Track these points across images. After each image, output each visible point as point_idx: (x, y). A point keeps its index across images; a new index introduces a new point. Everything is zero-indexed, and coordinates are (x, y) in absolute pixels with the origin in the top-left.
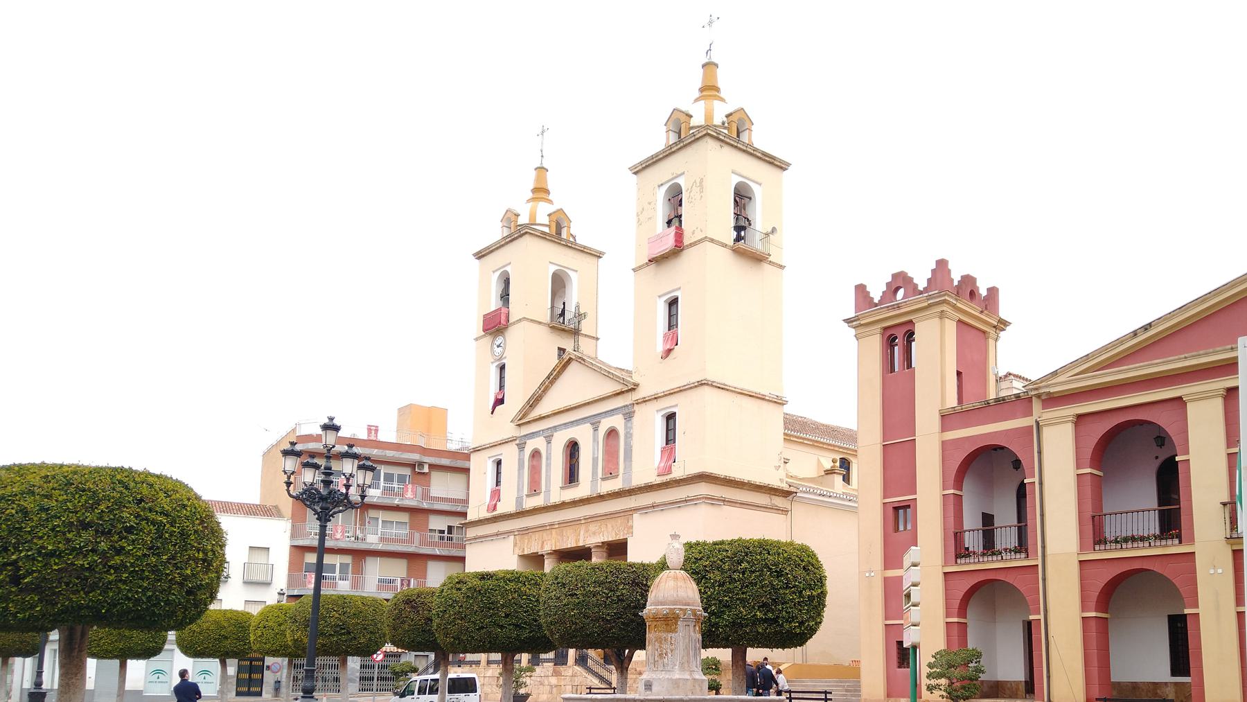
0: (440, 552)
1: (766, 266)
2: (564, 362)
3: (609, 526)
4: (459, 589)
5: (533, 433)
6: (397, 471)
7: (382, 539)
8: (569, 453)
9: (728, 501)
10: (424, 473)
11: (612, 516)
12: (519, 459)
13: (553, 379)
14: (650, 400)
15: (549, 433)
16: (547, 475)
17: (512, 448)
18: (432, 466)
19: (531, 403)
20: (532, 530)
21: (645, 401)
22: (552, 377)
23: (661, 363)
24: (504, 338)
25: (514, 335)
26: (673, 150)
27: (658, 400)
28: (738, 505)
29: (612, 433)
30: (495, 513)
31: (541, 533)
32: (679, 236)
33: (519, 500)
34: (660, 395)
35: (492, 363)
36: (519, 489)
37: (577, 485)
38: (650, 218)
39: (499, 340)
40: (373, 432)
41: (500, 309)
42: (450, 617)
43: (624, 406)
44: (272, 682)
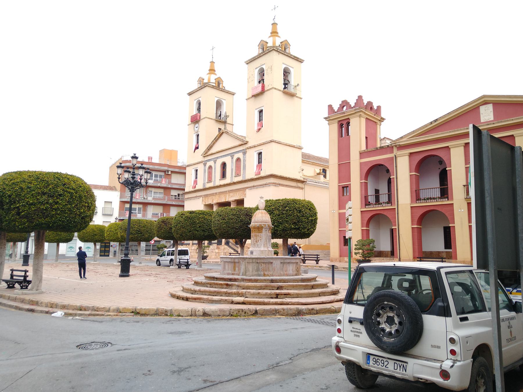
1: (295, 98)
2: (221, 133)
3: (237, 194)
4: (182, 217)
6: (159, 174)
7: (153, 199)
8: (222, 167)
9: (281, 185)
10: (169, 174)
12: (204, 169)
13: (216, 139)
14: (252, 147)
16: (214, 175)
18: (172, 172)
21: (250, 148)
23: (257, 134)
24: (199, 125)
25: (202, 123)
26: (261, 55)
28: (285, 186)
29: (238, 159)
30: (195, 189)
31: (212, 196)
32: (263, 87)
33: (204, 184)
34: (256, 145)
35: (194, 134)
36: (204, 180)
37: (225, 179)
38: (252, 80)
39: (197, 125)
40: (150, 159)
41: (197, 114)
42: (178, 227)
43: (243, 150)
44: (113, 251)
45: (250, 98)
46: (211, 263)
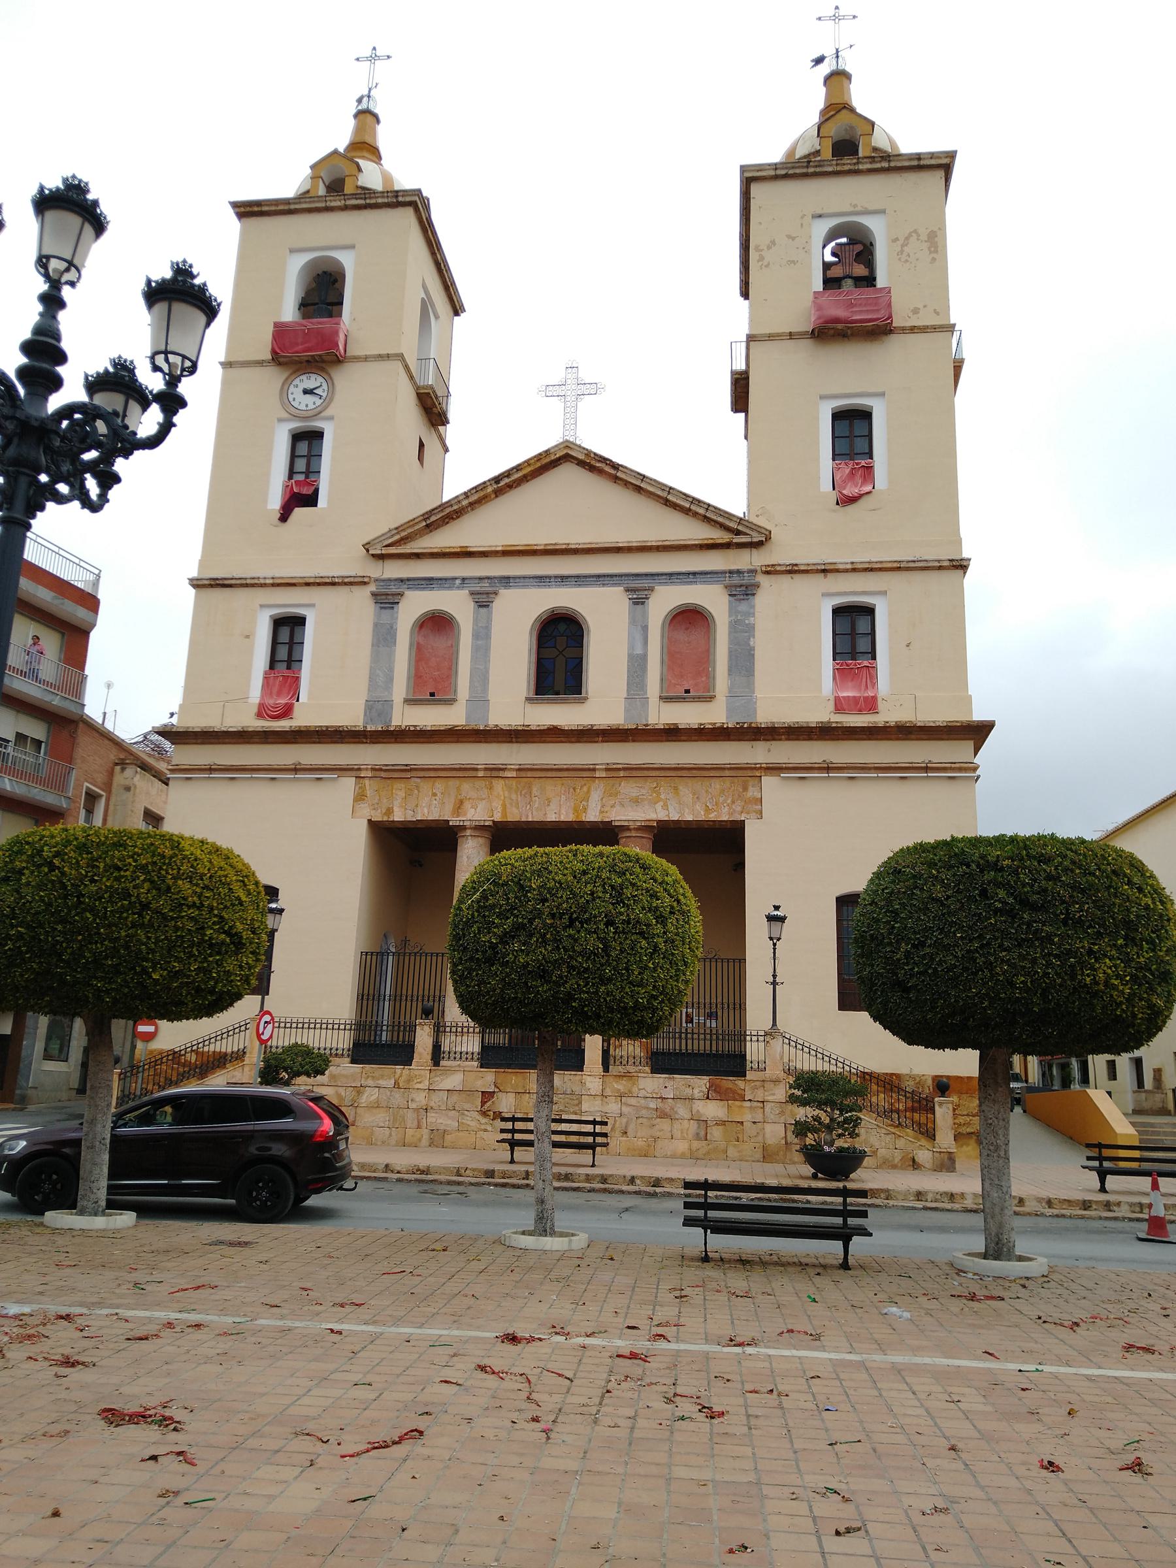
0: (12, 785)
3: (535, 791)
5: (431, 579)
11: (695, 773)
15: (485, 586)
17: (361, 601)
19: (433, 518)
20: (422, 774)
22: (506, 480)
23: (834, 511)
26: (861, 167)
27: (829, 575)
31: (457, 782)
33: (377, 705)
34: (841, 567)
35: (280, 420)
38: (793, 262)
43: (731, 572)
45: (779, 335)
46: (1124, 1211)
